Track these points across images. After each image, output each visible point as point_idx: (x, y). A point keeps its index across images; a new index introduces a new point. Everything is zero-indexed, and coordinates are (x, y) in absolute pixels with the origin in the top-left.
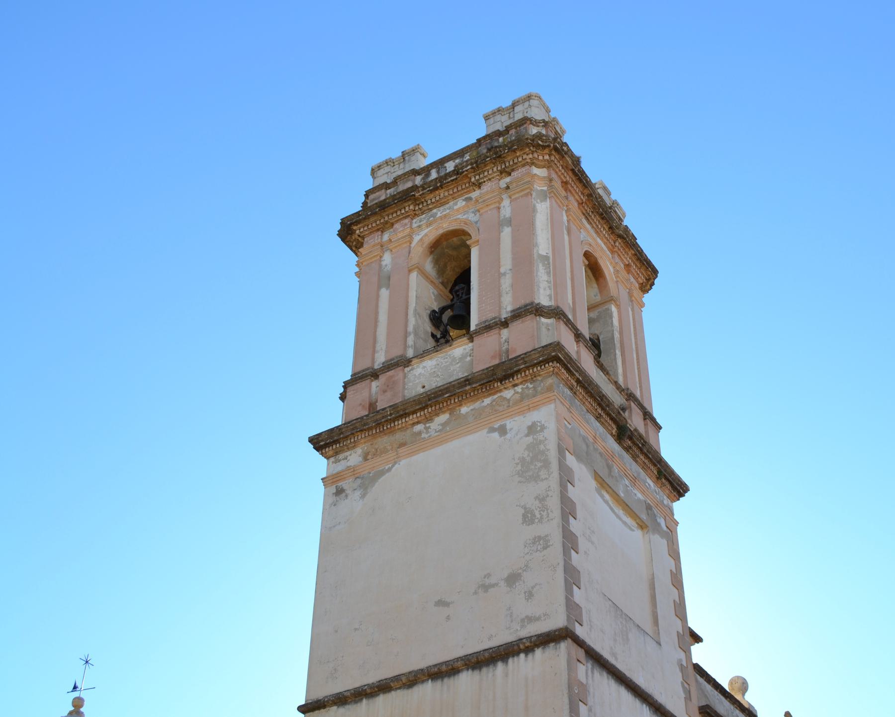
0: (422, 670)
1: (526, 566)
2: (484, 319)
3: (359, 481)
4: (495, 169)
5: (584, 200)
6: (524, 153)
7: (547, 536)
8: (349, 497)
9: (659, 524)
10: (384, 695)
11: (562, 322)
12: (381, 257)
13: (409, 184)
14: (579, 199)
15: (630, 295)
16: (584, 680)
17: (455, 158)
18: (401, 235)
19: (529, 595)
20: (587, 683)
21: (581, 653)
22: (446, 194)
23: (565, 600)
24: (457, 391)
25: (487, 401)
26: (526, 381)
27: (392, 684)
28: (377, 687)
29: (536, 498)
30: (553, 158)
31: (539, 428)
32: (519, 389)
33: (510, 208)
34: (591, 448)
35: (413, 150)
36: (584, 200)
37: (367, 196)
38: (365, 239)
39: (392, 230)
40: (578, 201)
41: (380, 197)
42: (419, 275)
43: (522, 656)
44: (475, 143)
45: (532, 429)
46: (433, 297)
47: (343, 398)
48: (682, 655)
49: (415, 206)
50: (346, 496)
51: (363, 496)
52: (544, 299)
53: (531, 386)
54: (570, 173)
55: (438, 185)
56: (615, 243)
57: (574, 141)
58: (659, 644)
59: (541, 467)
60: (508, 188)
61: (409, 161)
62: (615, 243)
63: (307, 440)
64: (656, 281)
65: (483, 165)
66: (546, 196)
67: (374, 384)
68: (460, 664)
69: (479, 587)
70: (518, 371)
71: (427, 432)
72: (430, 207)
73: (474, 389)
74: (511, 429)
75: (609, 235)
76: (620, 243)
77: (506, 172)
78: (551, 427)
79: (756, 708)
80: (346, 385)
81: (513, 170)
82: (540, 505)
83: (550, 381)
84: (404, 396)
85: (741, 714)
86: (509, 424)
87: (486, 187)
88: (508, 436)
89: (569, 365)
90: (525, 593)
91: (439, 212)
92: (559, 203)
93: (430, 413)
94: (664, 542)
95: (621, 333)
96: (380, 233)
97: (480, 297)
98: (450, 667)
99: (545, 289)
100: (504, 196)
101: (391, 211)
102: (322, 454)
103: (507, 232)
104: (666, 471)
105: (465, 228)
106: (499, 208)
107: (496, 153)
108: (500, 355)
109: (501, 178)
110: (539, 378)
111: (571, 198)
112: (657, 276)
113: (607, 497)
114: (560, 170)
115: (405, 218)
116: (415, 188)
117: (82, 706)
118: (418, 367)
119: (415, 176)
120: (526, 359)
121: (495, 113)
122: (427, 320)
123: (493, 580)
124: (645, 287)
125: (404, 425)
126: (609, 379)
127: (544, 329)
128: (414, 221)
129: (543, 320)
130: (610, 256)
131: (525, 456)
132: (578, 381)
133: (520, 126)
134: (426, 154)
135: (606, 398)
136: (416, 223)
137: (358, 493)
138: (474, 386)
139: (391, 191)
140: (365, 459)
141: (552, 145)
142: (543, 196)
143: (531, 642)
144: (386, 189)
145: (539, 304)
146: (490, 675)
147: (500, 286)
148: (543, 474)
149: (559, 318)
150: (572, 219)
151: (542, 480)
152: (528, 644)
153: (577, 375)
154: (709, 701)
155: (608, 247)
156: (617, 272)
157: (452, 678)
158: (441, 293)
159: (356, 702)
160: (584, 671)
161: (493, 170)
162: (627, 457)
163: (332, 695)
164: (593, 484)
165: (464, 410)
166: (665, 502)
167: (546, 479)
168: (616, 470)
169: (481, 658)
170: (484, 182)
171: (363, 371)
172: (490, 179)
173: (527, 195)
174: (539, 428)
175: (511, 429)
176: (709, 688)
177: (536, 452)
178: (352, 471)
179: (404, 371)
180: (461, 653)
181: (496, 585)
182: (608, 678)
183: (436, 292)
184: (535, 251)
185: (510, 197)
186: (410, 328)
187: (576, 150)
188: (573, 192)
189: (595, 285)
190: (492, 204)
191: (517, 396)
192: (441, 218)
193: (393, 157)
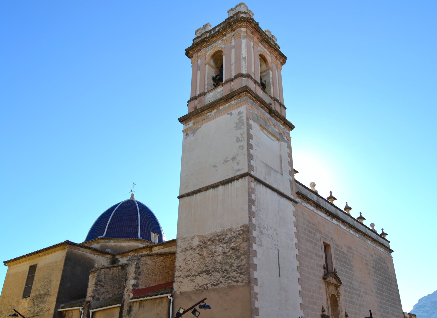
0: (209, 186)
1: (237, 155)
2: (226, 79)
3: (192, 131)
4: (230, 30)
5: (259, 37)
6: (238, 24)
7: (243, 146)
8: (190, 136)
9: (284, 139)
10: (200, 193)
11: (249, 79)
12: (198, 61)
13: (205, 36)
14: (258, 37)
15: (277, 66)
16: (253, 187)
17: (219, 27)
18: (203, 53)
19: (238, 163)
20: (255, 188)
21: (253, 179)
22: (216, 39)
23: (247, 165)
24: (218, 102)
25: (227, 105)
26: (238, 98)
27: (201, 190)
28: (198, 191)
29: (240, 134)
30: (247, 24)
31: (241, 113)
32: (236, 101)
33: (234, 42)
34: (259, 117)
35: (207, 25)
36: (259, 37)
37: (193, 41)
38: (193, 55)
39: (201, 52)
40: (257, 38)
41: (197, 41)
42: (209, 66)
43: (236, 181)
44: (224, 21)
45: (240, 113)
46: (214, 72)
47: (188, 106)
48: (291, 177)
49: (207, 43)
50: (189, 136)
51: (193, 136)
52: (244, 72)
53: (239, 100)
54: (254, 29)
55: (213, 36)
56: (271, 50)
57: (256, 18)
58: (282, 175)
59: (242, 125)
60: (234, 36)
61: (206, 28)
62: (271, 50)
63: (177, 120)
64: (287, 61)
65: (226, 29)
66: (245, 37)
67: (196, 101)
68: (219, 184)
69: (224, 161)
70: (236, 95)
71: (211, 115)
72: (211, 43)
73: (223, 102)
74: (234, 113)
75: (269, 47)
76: (273, 50)
77: (233, 30)
78: (245, 112)
79: (318, 191)
80: (188, 102)
81: (235, 29)
82: (241, 136)
83: (244, 98)
84: (204, 104)
85: (312, 193)
86: (233, 112)
87: (227, 36)
88: (233, 116)
89: (251, 92)
90: (237, 163)
91: (214, 45)
92: (250, 39)
93: (211, 110)
94: (286, 144)
95: (273, 79)
96: (197, 53)
97: (226, 72)
98: (217, 185)
99: (244, 68)
100: (233, 38)
101: (200, 46)
102: (182, 123)
103: (233, 50)
104: (286, 122)
105: (221, 50)
106: (231, 43)
107: (230, 24)
108: (231, 90)
109: (232, 32)
110: (242, 97)
111: (255, 37)
112: (286, 59)
113: (265, 132)
114: (250, 28)
115: (204, 47)
116: (206, 38)
117: (133, 196)
118: (208, 95)
119: (207, 33)
120: (237, 92)
121: (231, 10)
122: (211, 80)
123: (228, 159)
124: (283, 63)
125: (204, 114)
126: (267, 95)
127: (244, 82)
128: (207, 48)
129: (243, 78)
130: (270, 54)
131: (237, 121)
132: (254, 97)
133: (237, 14)
134: (211, 25)
135: (264, 101)
136: (207, 49)
137: (192, 135)
138: (223, 100)
139: (200, 39)
140: (194, 124)
141: (247, 20)
142: (244, 37)
143: (238, 177)
144: (199, 38)
145: (242, 73)
146: (227, 187)
147: (231, 68)
148: (242, 127)
149: (249, 77)
150: (255, 44)
151: (242, 129)
152: (237, 178)
153: (254, 95)
154: (299, 189)
155: (269, 52)
156: (272, 59)
157: (217, 188)
158: (216, 71)
159: (192, 195)
160: (253, 184)
161: (229, 30)
162: (273, 119)
163: (186, 194)
164: (259, 128)
165: (221, 108)
166: (287, 132)
167: (243, 128)
168: (268, 123)
169: (225, 182)
170: (227, 34)
171: (193, 97)
172: (228, 33)
173: (239, 38)
174: (241, 113)
175: (234, 113)
176: (300, 186)
177: (240, 119)
178: (190, 128)
179: (204, 97)
180: (220, 180)
181: (229, 160)
182: (263, 186)
183: (215, 71)
184: (241, 56)
185: (234, 39)
186: (206, 83)
187: (257, 20)
188: (255, 35)
189: (265, 64)
190: (229, 41)
191: (235, 103)
192: (215, 47)
193: (201, 27)
